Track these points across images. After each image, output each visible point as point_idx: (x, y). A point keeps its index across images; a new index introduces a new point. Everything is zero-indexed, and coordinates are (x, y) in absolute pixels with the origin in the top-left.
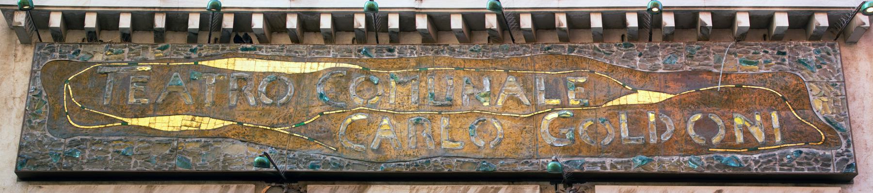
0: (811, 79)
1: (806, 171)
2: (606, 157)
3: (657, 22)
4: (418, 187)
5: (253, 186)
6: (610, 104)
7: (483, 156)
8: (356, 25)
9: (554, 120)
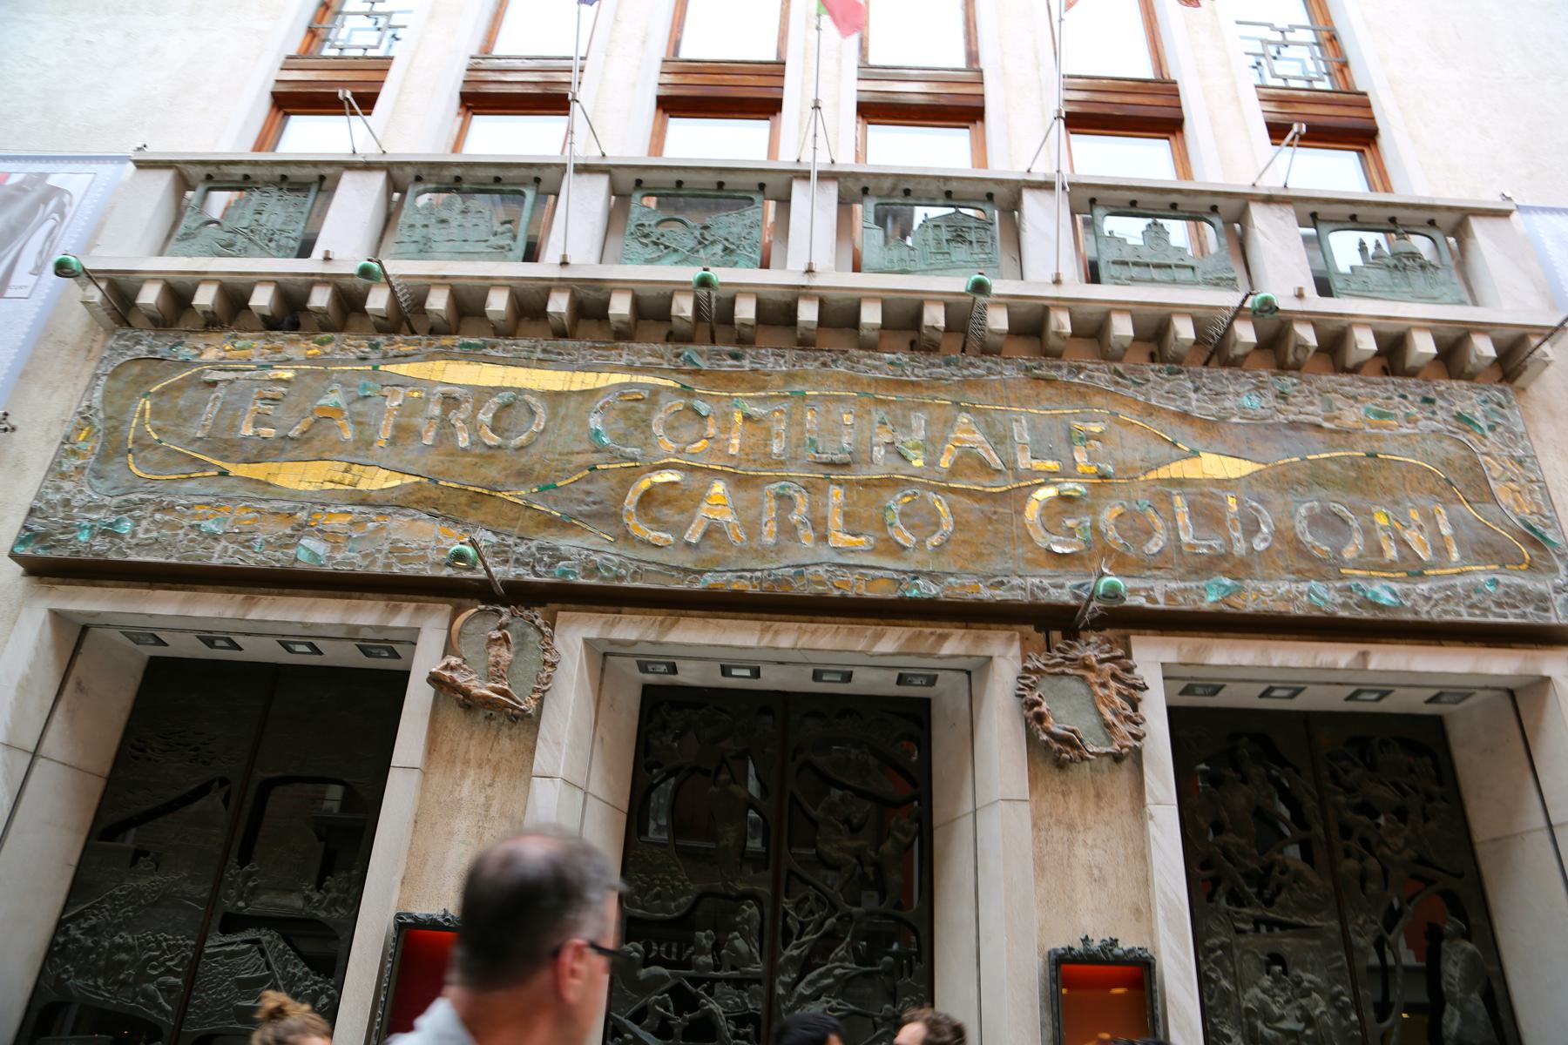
0: (1484, 449)
1: (1512, 620)
2: (1155, 577)
3: (419, 302)
4: (777, 625)
5: (448, 608)
6: (1152, 475)
7: (913, 567)
8: (674, 311)
9: (1051, 500)
